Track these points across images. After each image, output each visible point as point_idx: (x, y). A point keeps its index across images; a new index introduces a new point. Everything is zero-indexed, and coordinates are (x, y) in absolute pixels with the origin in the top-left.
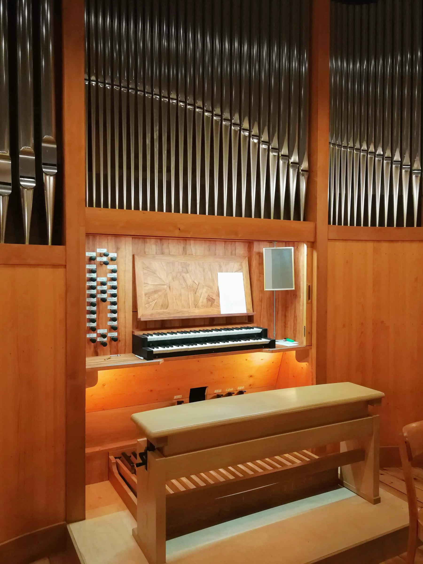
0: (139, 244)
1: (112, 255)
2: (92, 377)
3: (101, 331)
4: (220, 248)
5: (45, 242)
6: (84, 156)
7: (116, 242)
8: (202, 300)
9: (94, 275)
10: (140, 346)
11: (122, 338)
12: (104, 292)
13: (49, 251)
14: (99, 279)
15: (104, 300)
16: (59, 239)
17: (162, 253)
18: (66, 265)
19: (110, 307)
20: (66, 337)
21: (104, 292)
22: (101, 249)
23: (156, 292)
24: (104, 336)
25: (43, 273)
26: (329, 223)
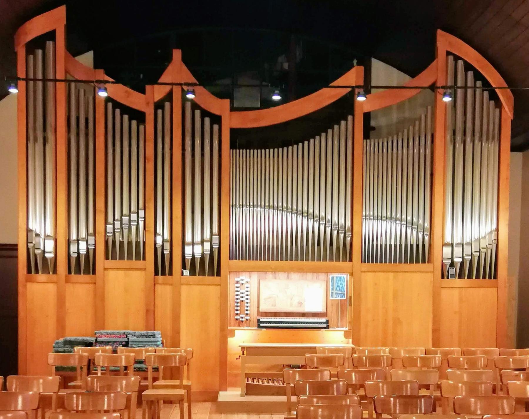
0: (262, 275)
1: (248, 280)
2: (232, 334)
3: (241, 316)
4: (309, 275)
5: (213, 275)
6: (355, 164)
7: (250, 274)
8: (295, 302)
9: (238, 289)
10: (259, 325)
11: (252, 319)
12: (242, 297)
13: (216, 279)
14: (241, 291)
15: (242, 301)
16: (219, 274)
17: (275, 279)
18: (352, 273)
19: (246, 305)
20: (154, 292)
21: (242, 297)
22: (244, 277)
23: (270, 298)
24: (242, 318)
25: (212, 288)
26: (362, 262)
